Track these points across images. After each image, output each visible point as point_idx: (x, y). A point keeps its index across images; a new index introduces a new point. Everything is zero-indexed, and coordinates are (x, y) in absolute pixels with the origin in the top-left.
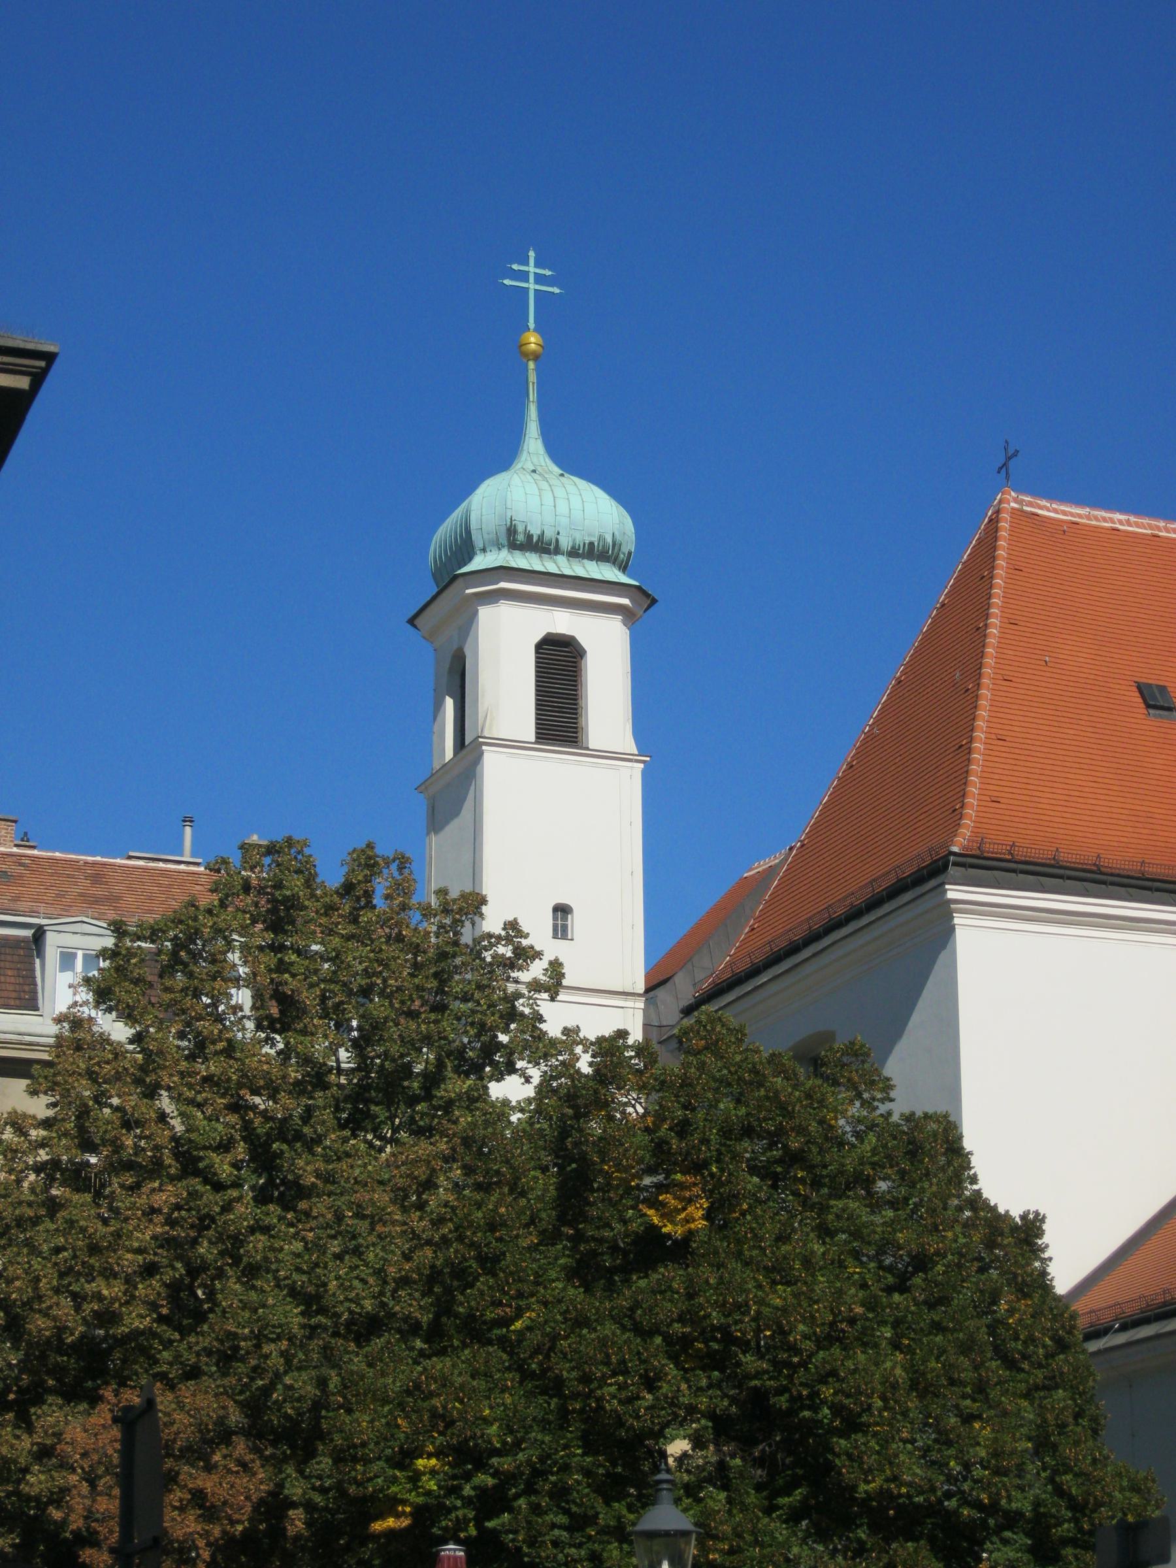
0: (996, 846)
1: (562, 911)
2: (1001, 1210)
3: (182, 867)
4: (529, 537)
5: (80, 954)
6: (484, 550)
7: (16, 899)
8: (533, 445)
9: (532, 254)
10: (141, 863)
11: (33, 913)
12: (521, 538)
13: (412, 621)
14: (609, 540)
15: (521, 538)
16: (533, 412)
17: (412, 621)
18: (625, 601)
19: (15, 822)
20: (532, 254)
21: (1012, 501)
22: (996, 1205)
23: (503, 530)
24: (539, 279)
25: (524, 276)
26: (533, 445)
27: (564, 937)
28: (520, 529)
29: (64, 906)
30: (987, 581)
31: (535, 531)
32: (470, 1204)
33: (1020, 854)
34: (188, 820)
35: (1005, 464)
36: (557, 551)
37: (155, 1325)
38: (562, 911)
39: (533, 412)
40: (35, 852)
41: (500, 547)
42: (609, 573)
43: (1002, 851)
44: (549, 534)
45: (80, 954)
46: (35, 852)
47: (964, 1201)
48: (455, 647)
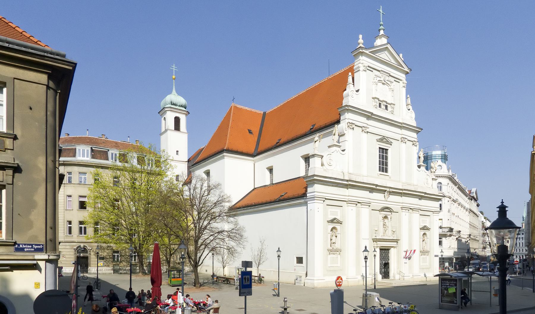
0: (230, 148)
1: (177, 151)
2: (461, 192)
3: (128, 143)
5: (114, 153)
8: (174, 91)
9: (174, 65)
10: (122, 142)
11: (108, 148)
12: (172, 103)
13: (158, 113)
15: (172, 103)
16: (174, 87)
17: (158, 113)
18: (186, 113)
20: (174, 65)
22: (13, 272)
23: (170, 102)
24: (175, 68)
25: (173, 68)
26: (174, 91)
27: (178, 155)
29: (112, 147)
30: (230, 114)
33: (233, 150)
34: (129, 137)
36: (177, 106)
38: (177, 151)
39: (174, 87)
40: (108, 140)
42: (184, 109)
43: (231, 149)
45: (114, 153)
46: (108, 140)
47: (492, 263)
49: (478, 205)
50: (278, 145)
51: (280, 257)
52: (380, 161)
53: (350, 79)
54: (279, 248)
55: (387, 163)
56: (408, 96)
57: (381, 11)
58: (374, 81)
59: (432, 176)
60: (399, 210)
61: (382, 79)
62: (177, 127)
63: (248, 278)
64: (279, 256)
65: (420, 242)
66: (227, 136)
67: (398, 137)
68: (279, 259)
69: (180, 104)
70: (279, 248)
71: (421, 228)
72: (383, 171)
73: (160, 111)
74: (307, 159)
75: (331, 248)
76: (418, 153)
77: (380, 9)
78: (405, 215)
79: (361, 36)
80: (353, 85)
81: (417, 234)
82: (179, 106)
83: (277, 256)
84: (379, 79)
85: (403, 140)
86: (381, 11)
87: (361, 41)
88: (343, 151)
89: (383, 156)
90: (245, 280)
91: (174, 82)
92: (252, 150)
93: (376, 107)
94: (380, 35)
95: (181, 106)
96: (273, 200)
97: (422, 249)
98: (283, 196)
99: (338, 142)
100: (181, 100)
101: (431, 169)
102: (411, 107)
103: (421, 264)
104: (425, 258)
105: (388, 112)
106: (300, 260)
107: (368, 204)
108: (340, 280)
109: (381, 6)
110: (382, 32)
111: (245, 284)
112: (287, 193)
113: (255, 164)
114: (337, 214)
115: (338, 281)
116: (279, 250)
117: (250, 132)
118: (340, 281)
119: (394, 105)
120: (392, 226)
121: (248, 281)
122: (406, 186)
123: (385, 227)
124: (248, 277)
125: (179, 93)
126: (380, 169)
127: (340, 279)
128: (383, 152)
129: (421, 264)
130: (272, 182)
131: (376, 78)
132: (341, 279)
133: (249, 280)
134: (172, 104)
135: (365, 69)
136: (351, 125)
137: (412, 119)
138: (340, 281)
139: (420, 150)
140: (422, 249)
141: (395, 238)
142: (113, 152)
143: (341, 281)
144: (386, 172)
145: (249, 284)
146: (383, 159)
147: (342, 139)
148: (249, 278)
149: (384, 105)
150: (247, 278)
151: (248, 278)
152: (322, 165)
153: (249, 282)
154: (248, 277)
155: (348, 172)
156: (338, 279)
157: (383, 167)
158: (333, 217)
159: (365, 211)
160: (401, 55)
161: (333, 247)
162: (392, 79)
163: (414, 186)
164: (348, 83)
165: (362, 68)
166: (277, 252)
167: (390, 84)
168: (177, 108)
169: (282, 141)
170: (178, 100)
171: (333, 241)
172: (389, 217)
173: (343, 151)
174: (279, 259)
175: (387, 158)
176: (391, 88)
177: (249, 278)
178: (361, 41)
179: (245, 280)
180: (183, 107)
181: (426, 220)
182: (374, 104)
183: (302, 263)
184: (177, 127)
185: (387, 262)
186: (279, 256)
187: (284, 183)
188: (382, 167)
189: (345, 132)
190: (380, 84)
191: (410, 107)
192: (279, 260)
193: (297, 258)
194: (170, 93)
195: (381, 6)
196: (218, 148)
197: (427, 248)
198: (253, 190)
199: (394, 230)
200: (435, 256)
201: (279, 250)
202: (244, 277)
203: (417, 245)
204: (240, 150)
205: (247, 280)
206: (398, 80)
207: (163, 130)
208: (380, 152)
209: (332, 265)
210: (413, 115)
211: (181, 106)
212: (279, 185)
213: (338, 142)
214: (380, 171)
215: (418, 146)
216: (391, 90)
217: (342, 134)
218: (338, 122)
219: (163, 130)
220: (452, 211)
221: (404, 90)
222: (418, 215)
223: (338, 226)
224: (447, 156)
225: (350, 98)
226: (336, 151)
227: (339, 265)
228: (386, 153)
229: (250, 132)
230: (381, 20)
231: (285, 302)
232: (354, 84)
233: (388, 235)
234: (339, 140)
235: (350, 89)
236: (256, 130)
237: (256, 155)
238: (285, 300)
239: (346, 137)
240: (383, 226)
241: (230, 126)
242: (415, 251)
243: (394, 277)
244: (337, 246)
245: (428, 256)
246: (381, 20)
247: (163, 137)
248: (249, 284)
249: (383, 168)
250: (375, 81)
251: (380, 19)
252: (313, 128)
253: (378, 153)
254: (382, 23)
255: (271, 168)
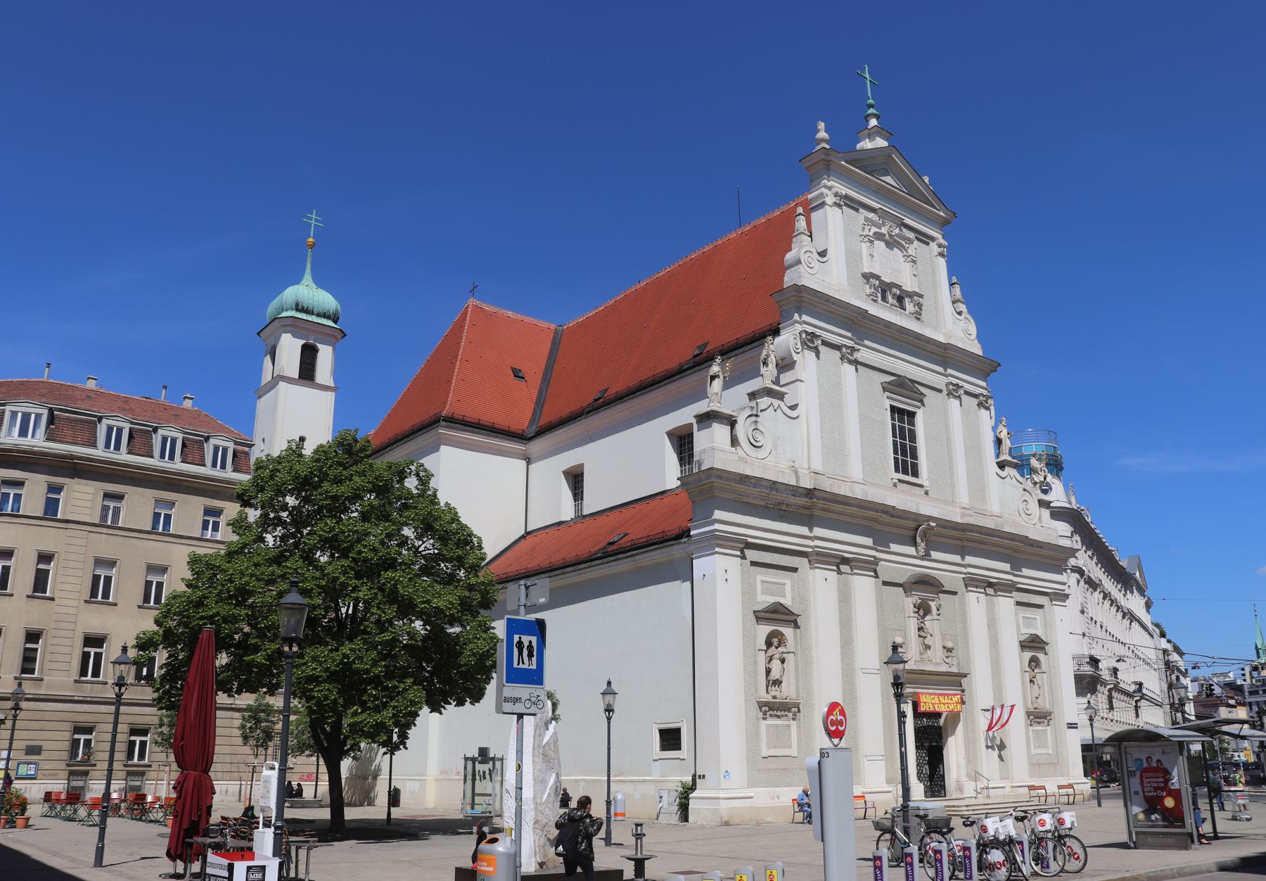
4: (303, 307)
6: (287, 310)
7: (92, 406)
8: (308, 276)
12: (300, 307)
14: (331, 312)
15: (300, 307)
16: (309, 266)
17: (258, 334)
19: (96, 379)
21: (472, 301)
24: (316, 220)
25: (311, 219)
26: (308, 276)
28: (300, 304)
30: (462, 327)
31: (305, 306)
32: (314, 608)
33: (466, 419)
34: (165, 387)
35: (473, 290)
36: (313, 314)
37: (349, 652)
41: (292, 309)
44: (310, 308)
48: (273, 343)
49: (1148, 606)
50: (601, 404)
51: (613, 710)
52: (897, 444)
53: (801, 223)
54: (609, 683)
55: (916, 450)
56: (954, 280)
57: (867, 75)
58: (864, 234)
59: (1036, 495)
60: (960, 587)
61: (884, 230)
62: (307, 372)
63: (530, 647)
64: (609, 710)
65: (1023, 683)
66: (449, 382)
67: (940, 381)
68: (609, 719)
69: (321, 310)
70: (609, 683)
71: (1022, 640)
72: (905, 472)
73: (265, 328)
74: (685, 439)
75: (769, 698)
76: (994, 429)
77: (864, 72)
78: (975, 602)
79: (821, 125)
80: (810, 239)
81: (1014, 659)
82: (318, 315)
83: (602, 708)
84: (874, 229)
85: (954, 391)
86: (867, 75)
87: (822, 134)
88: (793, 407)
89: (902, 429)
90: (520, 653)
91: (309, 254)
92: (522, 419)
93: (874, 298)
94: (869, 127)
95: (325, 315)
96: (585, 555)
97: (1030, 705)
98: (616, 542)
99: (777, 382)
100: (325, 300)
101: (1034, 476)
102: (964, 306)
103: (1033, 752)
104: (1043, 731)
105: (905, 314)
106: (670, 739)
107: (871, 567)
108: (837, 716)
109: (866, 66)
110: (873, 122)
111: (521, 666)
112: (627, 534)
113: (505, 711)
114: (785, 590)
115: (831, 717)
116: (609, 691)
117: (517, 374)
118: (840, 717)
119: (921, 296)
120: (942, 633)
121: (530, 655)
122: (971, 515)
123: (922, 634)
124: (530, 642)
125: (320, 282)
126: (898, 467)
127: (837, 710)
128: (901, 421)
129: (1033, 752)
130: (581, 511)
131: (867, 228)
132: (842, 713)
133: (535, 653)
134: (299, 308)
135: (838, 202)
136: (810, 341)
137: (969, 337)
138: (840, 717)
139: (998, 422)
140: (1030, 705)
141: (954, 670)
142: (111, 422)
143: (842, 717)
144: (915, 473)
145: (534, 667)
146: (903, 437)
147: (785, 378)
148: (534, 644)
149: (894, 295)
150: (526, 644)
151: (530, 647)
152: (734, 442)
153: (534, 659)
154: (530, 642)
155: (809, 469)
156: (830, 712)
157: (906, 460)
158: (772, 599)
159: (863, 585)
160: (926, 179)
161: (773, 693)
162: (911, 235)
163: (994, 517)
164: (796, 233)
165: (830, 200)
166: (603, 694)
167: (907, 246)
168: (311, 320)
169: (611, 392)
170: (316, 299)
171: (775, 674)
172: (933, 604)
173: (793, 407)
174: (609, 719)
175: (915, 436)
176: (910, 253)
177: (534, 644)
178: (822, 134)
179: (520, 653)
180: (328, 318)
181: (1035, 619)
182: (868, 291)
183: (679, 748)
184: (307, 372)
185: (935, 744)
186: (609, 710)
187: (615, 513)
188: (902, 460)
189: (795, 357)
190: (880, 245)
191: (962, 307)
192: (609, 723)
193: (662, 732)
194: (297, 280)
195: (866, 66)
196: (425, 415)
197: (1045, 704)
198: (523, 537)
199: (950, 645)
200: (1069, 728)
201: (609, 691)
202: (516, 638)
203: (1015, 692)
204: (488, 418)
205: (525, 652)
206: (925, 239)
207: (267, 377)
208: (893, 419)
209: (772, 752)
210: (973, 329)
211: (325, 315)
212: (600, 519)
213: (777, 382)
214: (897, 470)
215: (992, 408)
216: (909, 259)
217: (786, 362)
218: (776, 332)
219: (267, 377)
220: (1091, 612)
221: (942, 264)
222: (1012, 601)
223: (788, 631)
224: (1061, 458)
225: (802, 269)
226: (771, 409)
227: (794, 751)
228: (912, 423)
229: (517, 374)
230: (870, 95)
231: (637, 839)
232: (811, 236)
233: (934, 661)
234: (778, 379)
235: (801, 248)
236: (534, 371)
237: (533, 434)
238: (637, 830)
239: (798, 372)
240: (917, 633)
241: (465, 331)
242: (1013, 707)
243: (960, 788)
244: (788, 691)
245: (1049, 728)
246: (870, 95)
247: (263, 403)
248: (534, 667)
249: (905, 463)
250: (866, 232)
251: (867, 94)
252: (701, 354)
253: (889, 422)
254: (871, 101)
255: (577, 472)
